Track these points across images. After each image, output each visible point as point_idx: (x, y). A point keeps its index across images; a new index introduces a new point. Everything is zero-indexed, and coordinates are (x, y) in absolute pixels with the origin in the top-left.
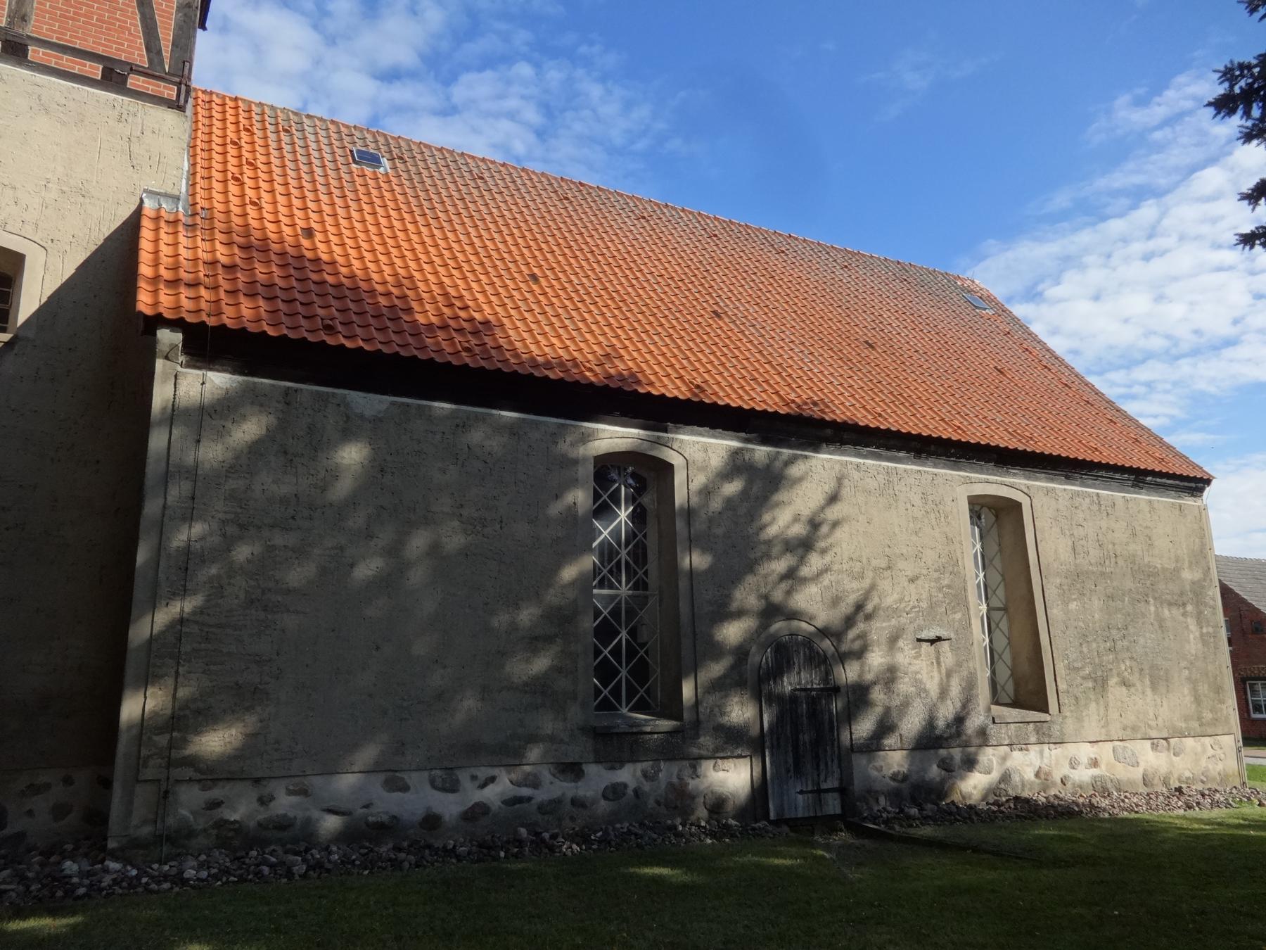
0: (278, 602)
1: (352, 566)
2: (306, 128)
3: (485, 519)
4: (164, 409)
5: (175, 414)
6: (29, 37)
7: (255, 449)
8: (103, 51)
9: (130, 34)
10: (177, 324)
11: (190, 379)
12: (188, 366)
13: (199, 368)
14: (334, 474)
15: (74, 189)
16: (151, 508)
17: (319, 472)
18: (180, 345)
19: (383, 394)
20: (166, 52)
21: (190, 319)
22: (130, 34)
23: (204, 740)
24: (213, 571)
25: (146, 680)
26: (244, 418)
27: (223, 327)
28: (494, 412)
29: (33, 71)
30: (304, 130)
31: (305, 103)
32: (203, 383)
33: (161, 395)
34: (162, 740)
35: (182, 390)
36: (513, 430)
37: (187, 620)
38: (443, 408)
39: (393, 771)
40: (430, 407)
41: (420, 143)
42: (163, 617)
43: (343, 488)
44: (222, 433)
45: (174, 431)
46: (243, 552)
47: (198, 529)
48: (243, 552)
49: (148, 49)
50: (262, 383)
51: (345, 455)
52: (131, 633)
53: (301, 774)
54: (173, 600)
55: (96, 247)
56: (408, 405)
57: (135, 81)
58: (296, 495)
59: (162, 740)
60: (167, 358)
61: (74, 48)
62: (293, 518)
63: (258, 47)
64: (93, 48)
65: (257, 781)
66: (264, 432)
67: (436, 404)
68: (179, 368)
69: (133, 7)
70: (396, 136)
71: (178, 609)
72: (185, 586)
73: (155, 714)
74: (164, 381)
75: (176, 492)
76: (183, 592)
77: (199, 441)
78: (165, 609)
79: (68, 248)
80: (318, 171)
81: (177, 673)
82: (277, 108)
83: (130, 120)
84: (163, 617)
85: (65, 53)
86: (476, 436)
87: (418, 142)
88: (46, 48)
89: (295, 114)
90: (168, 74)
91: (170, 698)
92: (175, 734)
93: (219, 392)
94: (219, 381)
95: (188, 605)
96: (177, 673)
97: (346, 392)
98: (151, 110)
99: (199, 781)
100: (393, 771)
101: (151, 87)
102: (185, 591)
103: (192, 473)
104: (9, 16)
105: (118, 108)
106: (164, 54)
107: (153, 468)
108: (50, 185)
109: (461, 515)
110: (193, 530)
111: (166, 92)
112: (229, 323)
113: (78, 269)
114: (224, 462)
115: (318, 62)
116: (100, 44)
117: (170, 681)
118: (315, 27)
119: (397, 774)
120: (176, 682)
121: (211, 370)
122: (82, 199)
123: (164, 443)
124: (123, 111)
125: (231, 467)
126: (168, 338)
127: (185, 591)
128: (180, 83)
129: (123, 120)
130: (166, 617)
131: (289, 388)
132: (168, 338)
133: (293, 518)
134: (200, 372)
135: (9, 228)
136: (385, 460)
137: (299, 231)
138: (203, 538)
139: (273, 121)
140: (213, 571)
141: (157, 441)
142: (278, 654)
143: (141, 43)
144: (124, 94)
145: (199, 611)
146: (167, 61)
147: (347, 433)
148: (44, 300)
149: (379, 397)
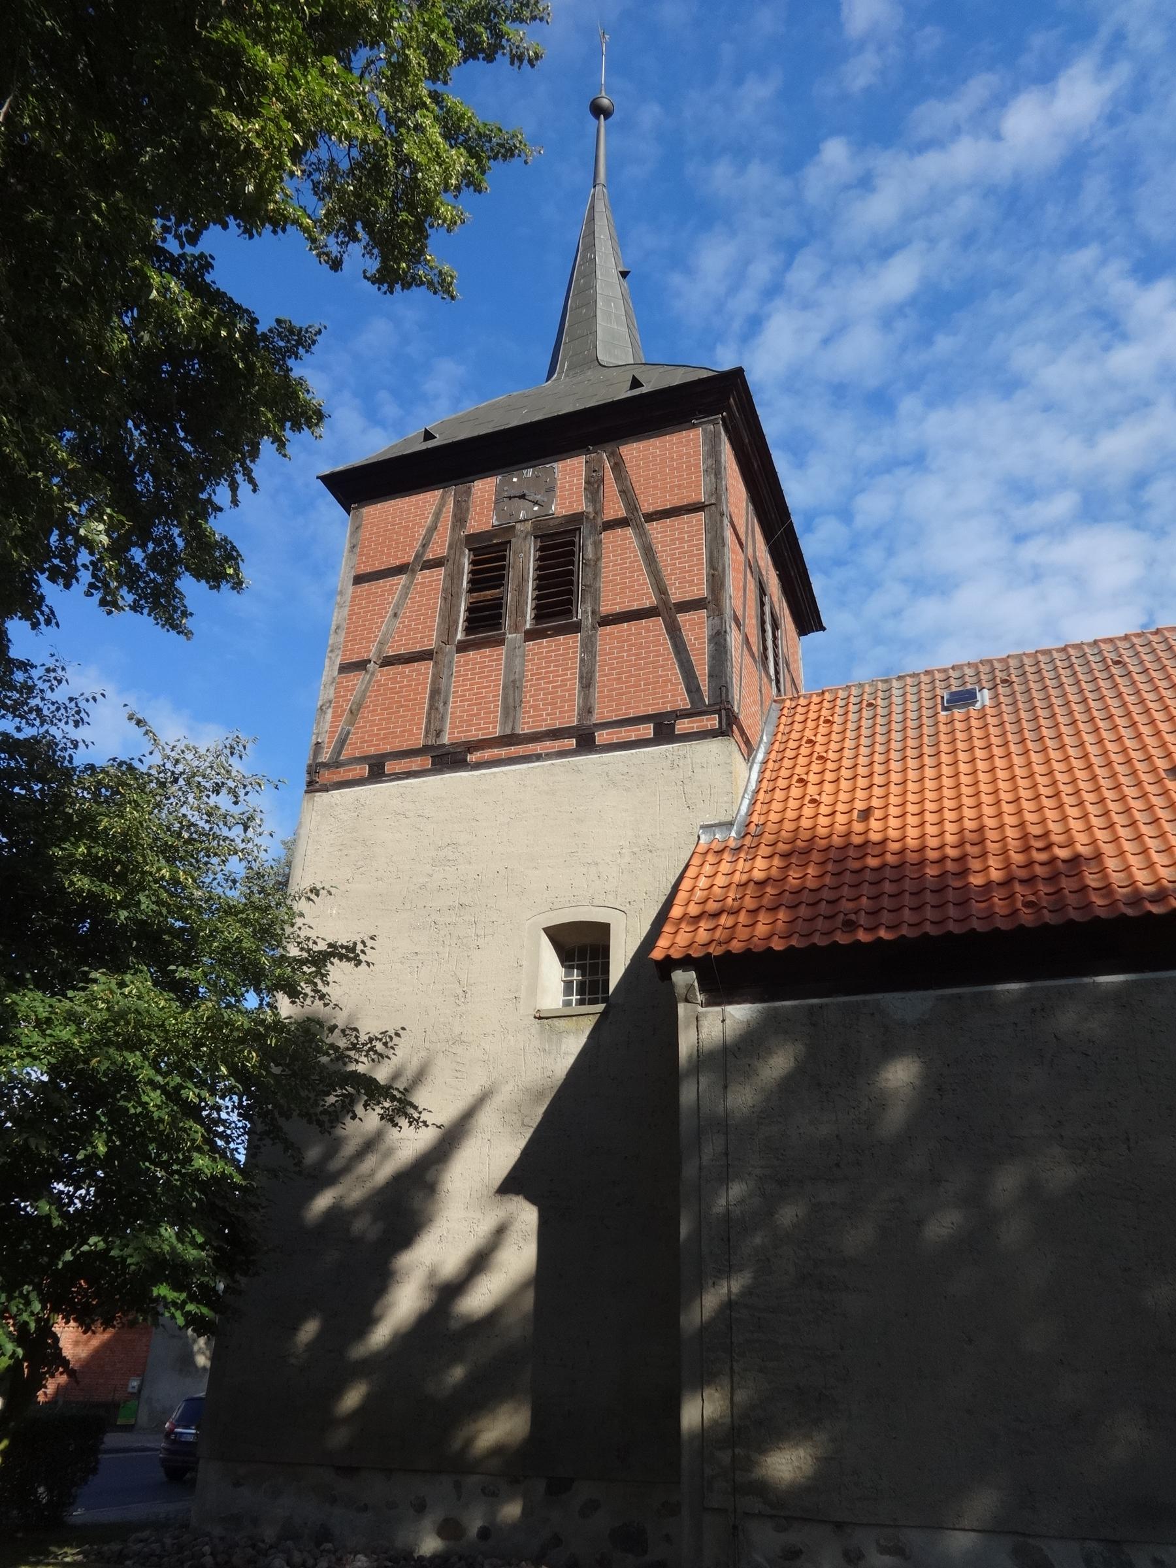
0: (834, 1277)
1: (920, 1223)
2: (1156, 646)
3: (1100, 1138)
4: (690, 1056)
5: (705, 1060)
6: (595, 725)
7: (788, 1085)
8: (653, 710)
9: (672, 684)
10: (686, 962)
11: (710, 1017)
12: (709, 1003)
13: (719, 1004)
14: (881, 1103)
15: (642, 848)
16: (689, 1171)
17: (860, 1102)
18: (696, 984)
19: (926, 989)
20: (705, 688)
21: (696, 954)
22: (672, 684)
23: (769, 1460)
24: (758, 1240)
25: (701, 1382)
26: (770, 1052)
27: (1071, 923)
28: (1087, 980)
29: (600, 753)
30: (1154, 650)
31: (1151, 614)
32: (723, 1021)
33: (686, 1043)
34: (725, 1457)
35: (704, 1032)
36: (1118, 996)
37: (736, 1303)
38: (1008, 991)
39: (1023, 1534)
40: (990, 993)
41: (1037, 652)
42: (711, 1300)
43: (895, 1118)
44: (749, 1072)
45: (702, 1080)
46: (788, 1215)
47: (737, 1190)
48: (788, 1215)
49: (689, 691)
50: (783, 1006)
51: (890, 1076)
52: (683, 1320)
53: (892, 1523)
54: (719, 1278)
55: (665, 897)
56: (959, 997)
57: (682, 726)
58: (837, 1136)
59: (725, 1457)
60: (687, 1000)
61: (629, 718)
62: (838, 1165)
63: (1078, 579)
64: (644, 711)
65: (839, 1526)
66: (792, 1064)
67: (1000, 987)
68: (700, 1009)
69: (672, 658)
70: (1004, 656)
71: (725, 1290)
72: (729, 1261)
73: (715, 1423)
74: (687, 1027)
75: (710, 1150)
76: (727, 1270)
77: (726, 1087)
78: (712, 1290)
79: (642, 906)
80: (896, 736)
81: (732, 1369)
82: (962, 665)
83: (681, 764)
84: (711, 1300)
85: (623, 727)
86: (1067, 1019)
87: (1034, 651)
88: (608, 729)
89: (1138, 635)
90: (710, 705)
91: (728, 1402)
92: (737, 1451)
93: (741, 1026)
94: (740, 1013)
95: (736, 1285)
96: (732, 1369)
97: (879, 996)
98: (698, 747)
99: (771, 1517)
100: (1023, 1534)
101: (695, 725)
102: (730, 1267)
103: (723, 1124)
104: (579, 714)
105: (670, 757)
106: (702, 688)
107: (686, 1124)
108: (624, 850)
109: (1062, 1136)
110: (731, 1192)
111: (709, 723)
112: (1102, 913)
113: (652, 925)
114: (754, 1106)
115: (1151, 563)
116: (649, 705)
117: (726, 1381)
118: (1137, 527)
119: (1030, 1541)
120: (732, 1382)
121: (730, 1003)
122: (650, 854)
123: (693, 1096)
124: (675, 757)
125: (761, 1111)
126: (683, 978)
127: (730, 1267)
128: (720, 710)
129: (675, 766)
130: (485, 1290)
131: (812, 1006)
132: (683, 978)
133: (838, 1165)
134: (718, 1009)
135: (596, 902)
136: (941, 1075)
137: (1163, 775)
138: (742, 1201)
139: (1098, 659)
140: (758, 1240)
141: (688, 1094)
142: (842, 1348)
143: (682, 689)
144: (673, 742)
145: (748, 1292)
146: (706, 694)
147: (889, 1050)
148: (628, 962)
149: (921, 993)
